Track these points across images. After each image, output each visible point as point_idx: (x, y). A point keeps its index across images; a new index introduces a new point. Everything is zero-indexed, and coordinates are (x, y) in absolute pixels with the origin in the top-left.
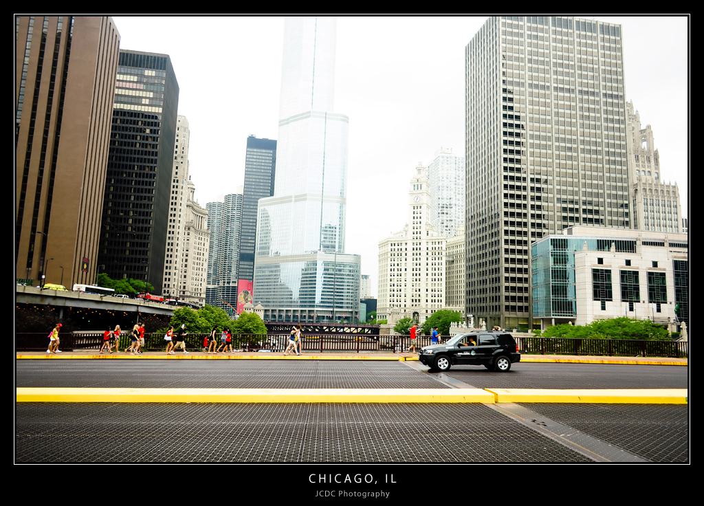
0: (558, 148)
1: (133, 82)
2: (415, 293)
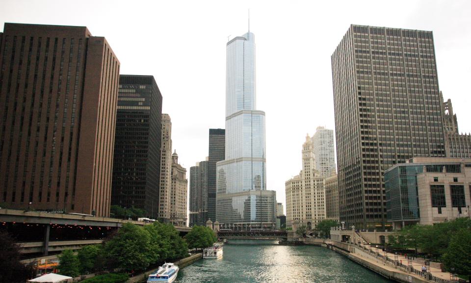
1: (133, 93)
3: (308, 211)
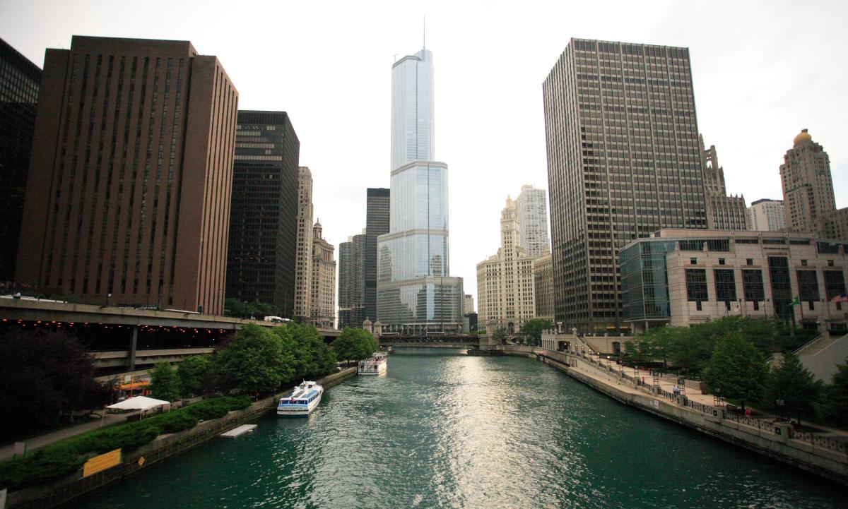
0: (636, 164)
1: (258, 137)
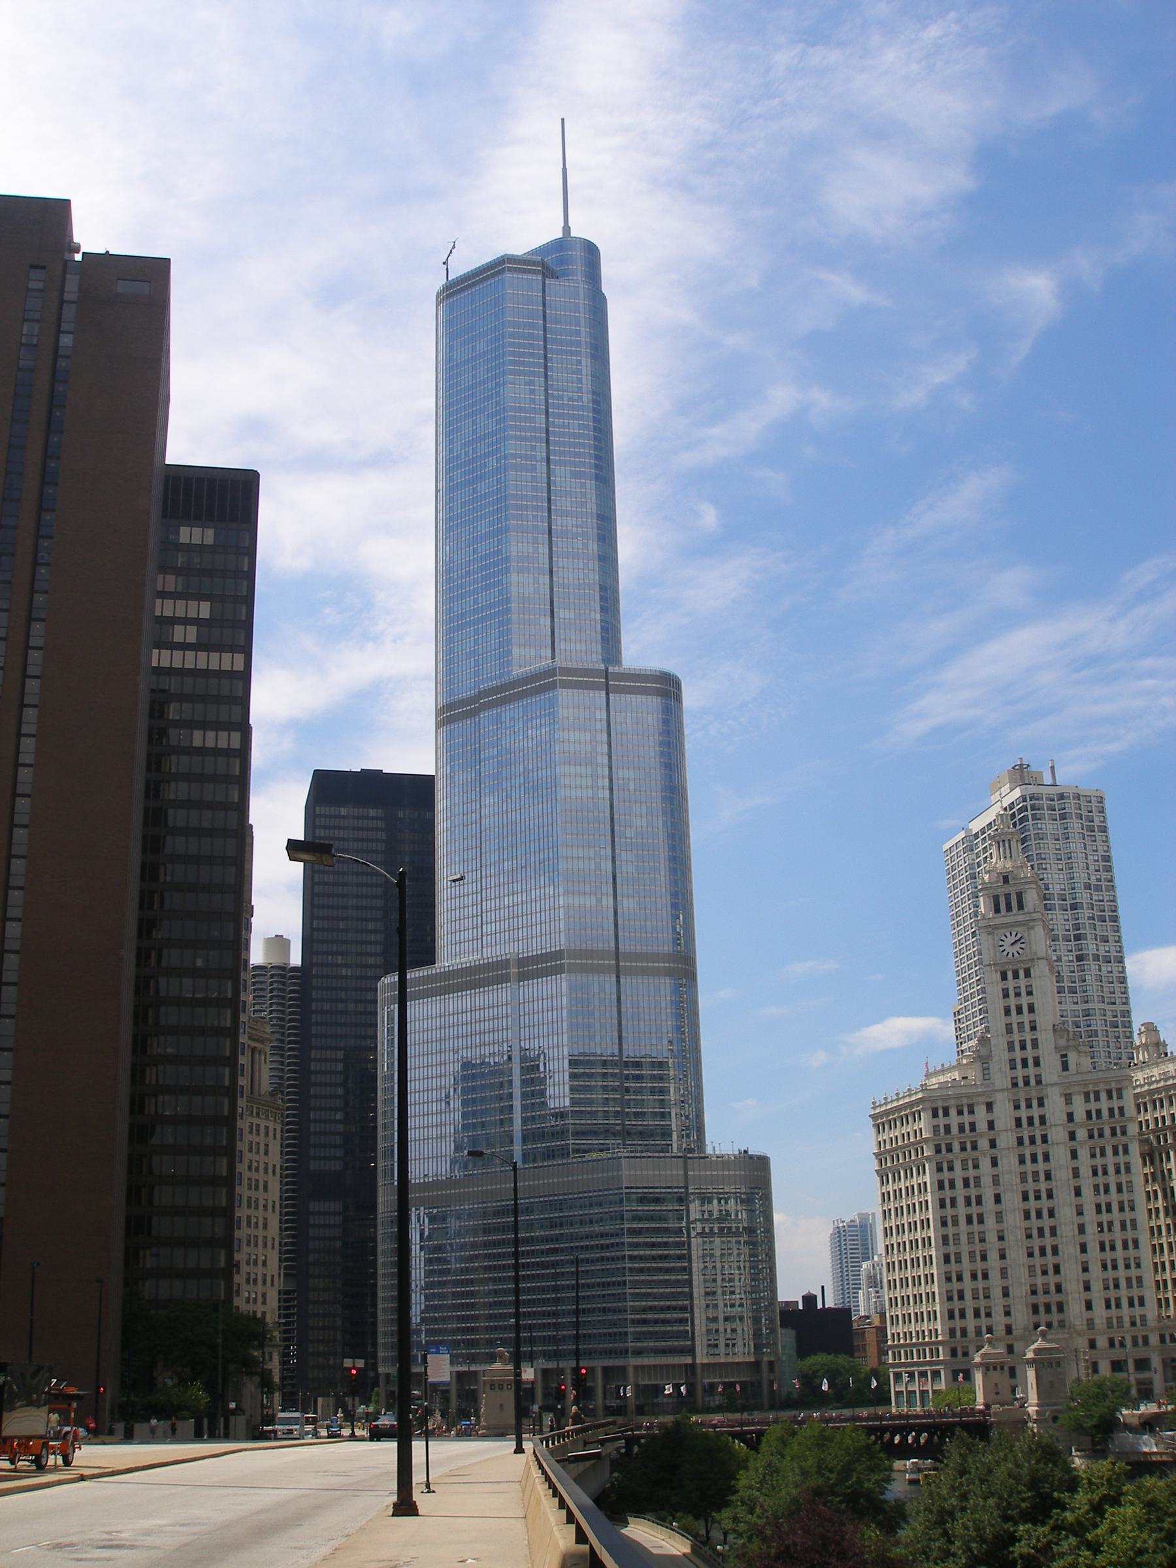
2: (1040, 1280)
3: (1040, 1280)
